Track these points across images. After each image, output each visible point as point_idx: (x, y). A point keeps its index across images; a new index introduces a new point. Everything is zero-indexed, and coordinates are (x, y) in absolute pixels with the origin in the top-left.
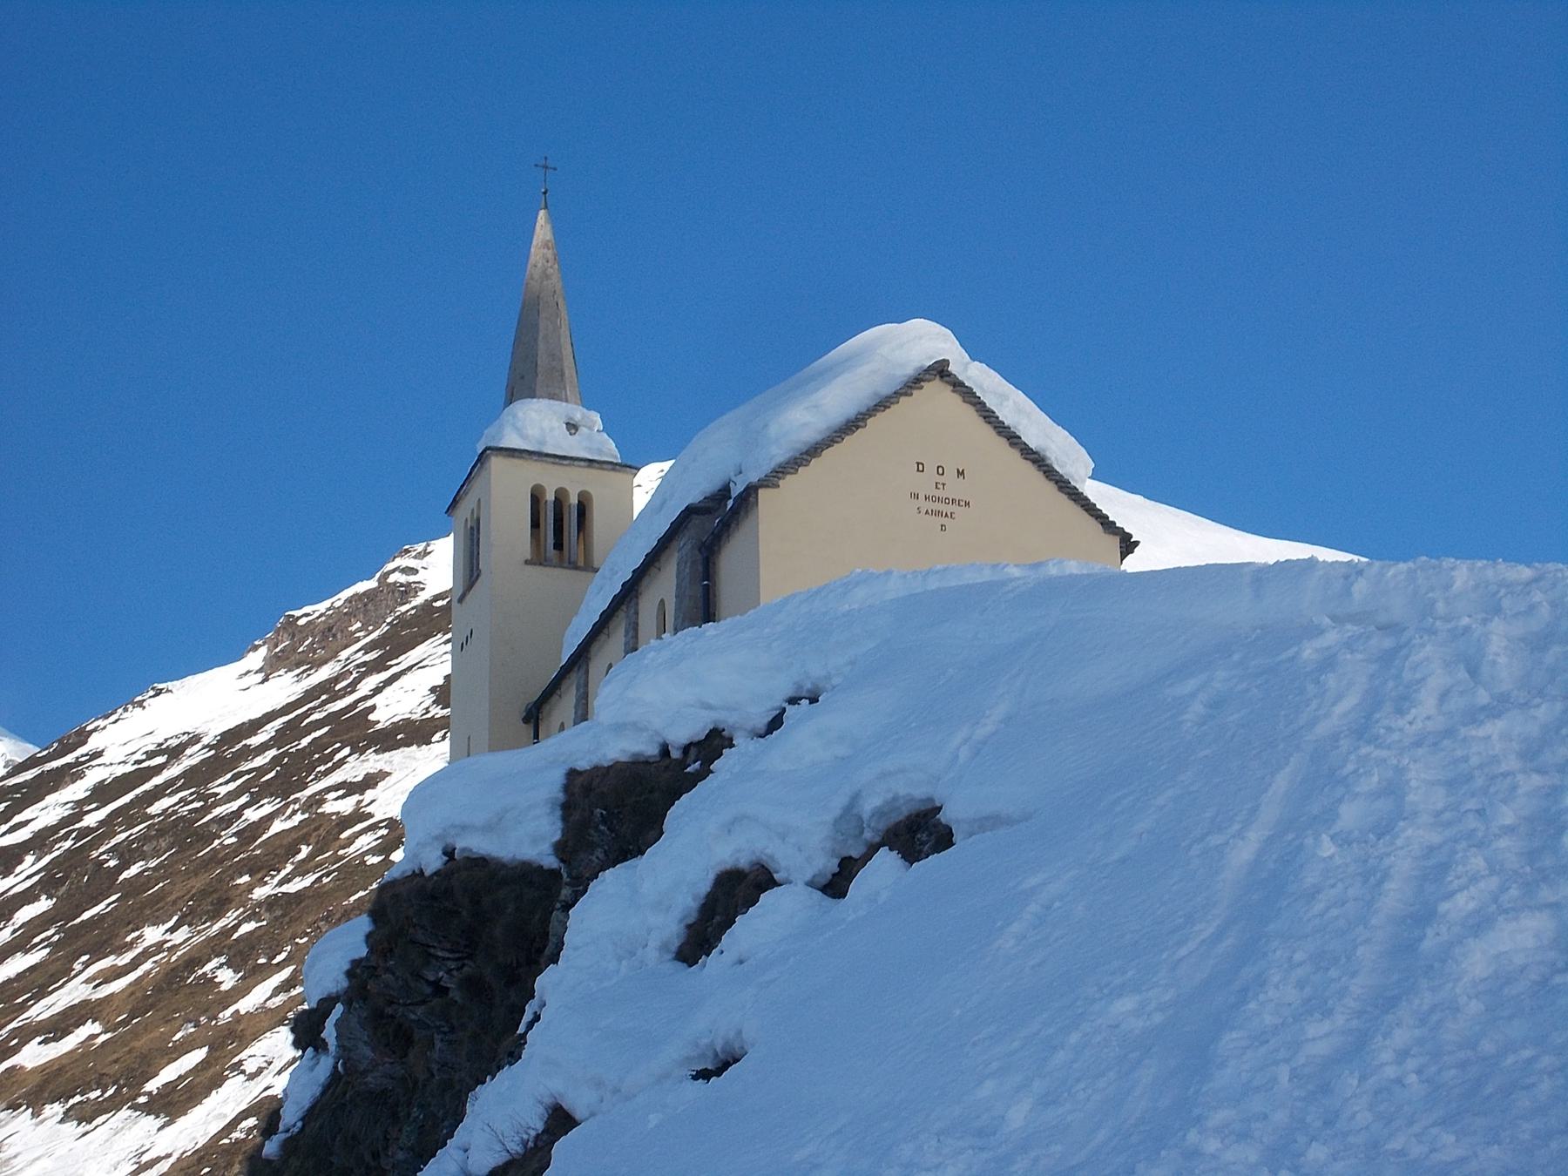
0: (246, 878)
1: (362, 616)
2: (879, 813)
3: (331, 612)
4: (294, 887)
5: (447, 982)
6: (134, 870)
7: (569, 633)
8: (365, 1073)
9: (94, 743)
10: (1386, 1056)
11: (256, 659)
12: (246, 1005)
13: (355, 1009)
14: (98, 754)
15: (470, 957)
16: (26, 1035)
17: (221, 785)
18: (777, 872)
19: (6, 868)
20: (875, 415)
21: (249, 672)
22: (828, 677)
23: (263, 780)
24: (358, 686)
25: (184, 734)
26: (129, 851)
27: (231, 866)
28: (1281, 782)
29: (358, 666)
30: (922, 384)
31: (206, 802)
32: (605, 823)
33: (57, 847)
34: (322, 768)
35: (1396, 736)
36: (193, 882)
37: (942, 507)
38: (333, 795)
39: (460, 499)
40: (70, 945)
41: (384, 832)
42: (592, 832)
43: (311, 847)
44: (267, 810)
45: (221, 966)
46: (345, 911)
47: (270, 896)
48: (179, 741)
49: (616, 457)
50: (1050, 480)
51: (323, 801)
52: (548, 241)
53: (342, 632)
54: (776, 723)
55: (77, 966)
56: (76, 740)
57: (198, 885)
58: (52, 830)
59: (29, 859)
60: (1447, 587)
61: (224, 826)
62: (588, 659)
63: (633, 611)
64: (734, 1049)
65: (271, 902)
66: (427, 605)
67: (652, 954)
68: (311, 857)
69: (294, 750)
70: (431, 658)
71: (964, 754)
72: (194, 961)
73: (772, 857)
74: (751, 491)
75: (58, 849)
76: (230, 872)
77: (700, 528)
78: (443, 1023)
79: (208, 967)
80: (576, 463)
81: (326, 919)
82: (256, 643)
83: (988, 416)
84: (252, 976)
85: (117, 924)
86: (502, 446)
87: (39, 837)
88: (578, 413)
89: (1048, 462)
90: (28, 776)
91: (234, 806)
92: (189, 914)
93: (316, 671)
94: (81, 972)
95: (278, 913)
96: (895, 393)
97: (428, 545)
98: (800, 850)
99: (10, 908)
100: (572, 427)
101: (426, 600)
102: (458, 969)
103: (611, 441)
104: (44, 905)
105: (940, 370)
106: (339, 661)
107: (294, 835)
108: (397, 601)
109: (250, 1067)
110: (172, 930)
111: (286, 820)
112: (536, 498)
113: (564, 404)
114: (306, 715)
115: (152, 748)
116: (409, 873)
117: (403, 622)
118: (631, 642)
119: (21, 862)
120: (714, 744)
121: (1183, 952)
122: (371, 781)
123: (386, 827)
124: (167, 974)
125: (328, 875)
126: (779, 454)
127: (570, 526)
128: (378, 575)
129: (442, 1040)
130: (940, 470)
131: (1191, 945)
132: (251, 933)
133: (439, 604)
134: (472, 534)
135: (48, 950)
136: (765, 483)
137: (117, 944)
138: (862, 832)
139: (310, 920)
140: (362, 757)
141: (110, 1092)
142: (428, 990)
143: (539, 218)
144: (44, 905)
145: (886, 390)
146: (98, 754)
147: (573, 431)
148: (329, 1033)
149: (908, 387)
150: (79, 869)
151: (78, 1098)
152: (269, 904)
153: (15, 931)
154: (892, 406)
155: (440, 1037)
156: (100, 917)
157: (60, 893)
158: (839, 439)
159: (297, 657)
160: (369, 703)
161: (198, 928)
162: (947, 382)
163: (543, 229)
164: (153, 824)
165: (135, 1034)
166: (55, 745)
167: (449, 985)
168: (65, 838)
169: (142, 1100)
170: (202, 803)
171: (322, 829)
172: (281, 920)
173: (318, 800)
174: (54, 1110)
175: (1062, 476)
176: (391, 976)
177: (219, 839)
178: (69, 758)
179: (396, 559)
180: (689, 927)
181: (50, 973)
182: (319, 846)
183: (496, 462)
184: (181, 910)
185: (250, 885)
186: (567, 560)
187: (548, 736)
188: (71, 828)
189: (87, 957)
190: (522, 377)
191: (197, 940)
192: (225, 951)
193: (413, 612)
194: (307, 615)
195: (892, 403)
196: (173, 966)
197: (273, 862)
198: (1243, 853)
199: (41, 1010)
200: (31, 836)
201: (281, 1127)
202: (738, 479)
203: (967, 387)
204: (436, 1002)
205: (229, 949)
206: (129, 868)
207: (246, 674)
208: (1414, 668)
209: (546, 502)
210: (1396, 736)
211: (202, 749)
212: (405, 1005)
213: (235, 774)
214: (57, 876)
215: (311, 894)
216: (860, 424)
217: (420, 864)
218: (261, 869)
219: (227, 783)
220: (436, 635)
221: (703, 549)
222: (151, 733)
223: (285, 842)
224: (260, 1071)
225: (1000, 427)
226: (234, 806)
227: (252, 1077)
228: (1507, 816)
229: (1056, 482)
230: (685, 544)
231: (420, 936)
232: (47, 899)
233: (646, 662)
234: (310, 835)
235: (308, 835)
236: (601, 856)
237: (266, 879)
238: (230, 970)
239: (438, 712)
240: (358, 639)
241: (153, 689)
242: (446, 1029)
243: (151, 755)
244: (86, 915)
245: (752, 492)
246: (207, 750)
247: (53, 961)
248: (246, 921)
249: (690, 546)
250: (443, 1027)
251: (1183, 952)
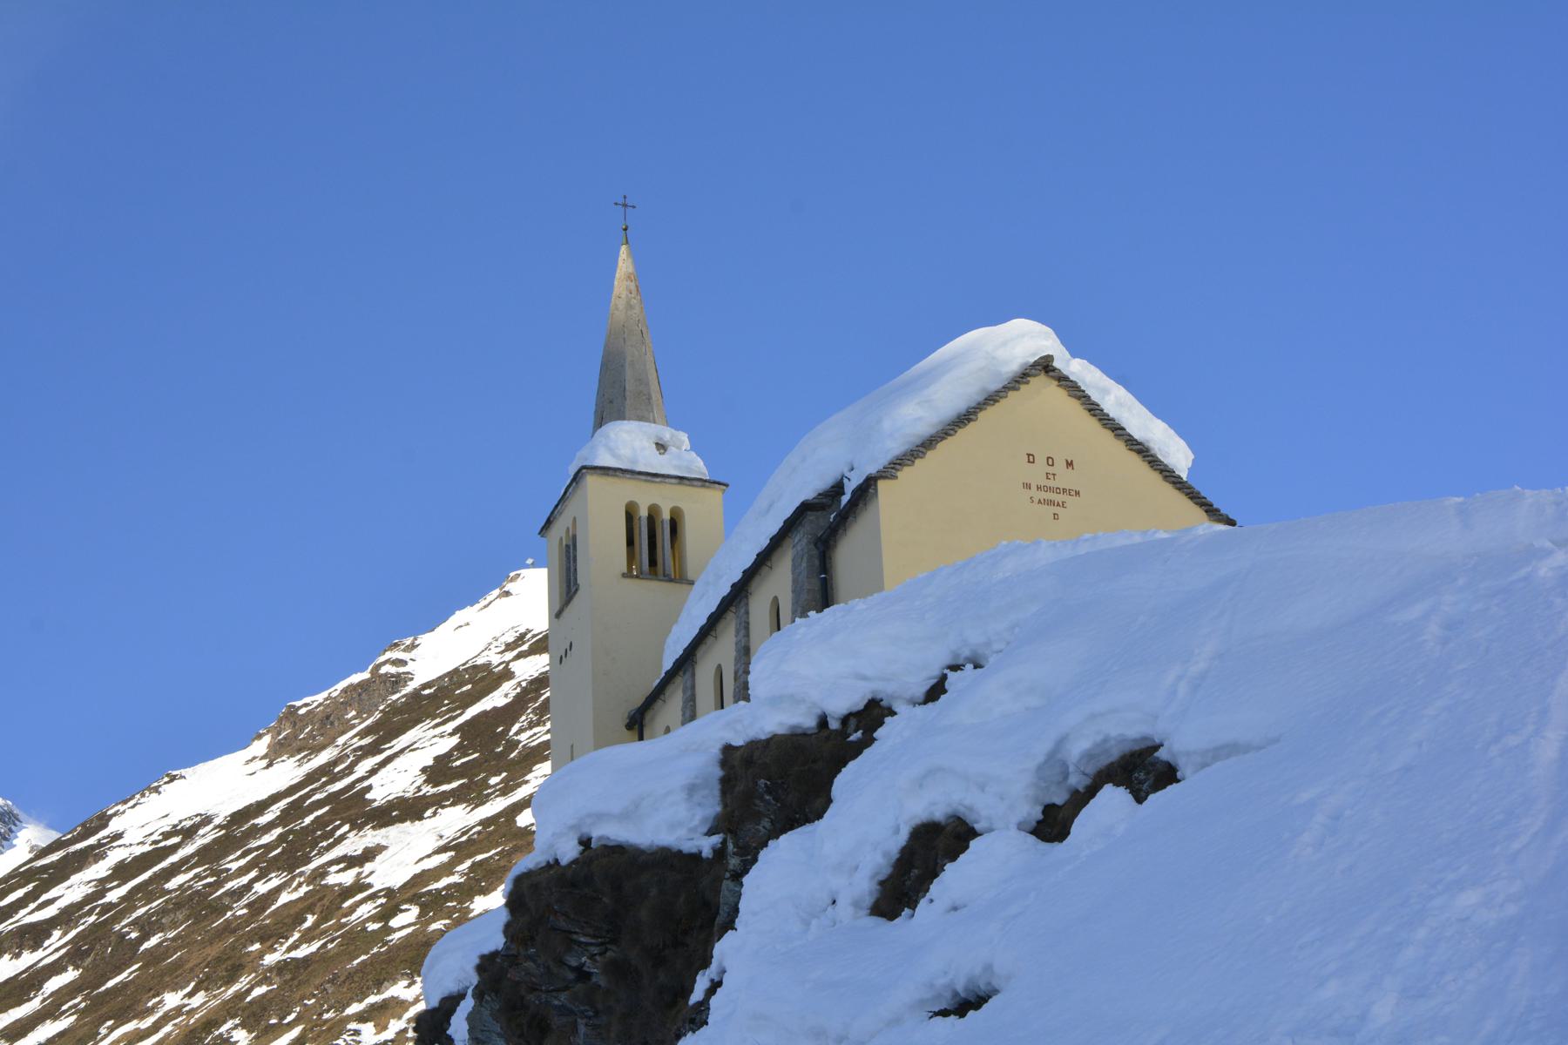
0: (257, 946)
1: (356, 705)
2: (1089, 756)
3: (328, 702)
4: (303, 952)
5: (590, 967)
6: (154, 941)
7: (670, 640)
9: (114, 826)
11: (261, 746)
13: (487, 1002)
14: (118, 836)
15: (614, 941)
17: (232, 861)
18: (977, 822)
19: (36, 943)
20: (986, 409)
21: (254, 758)
22: (988, 644)
23: (270, 856)
24: (356, 769)
25: (196, 816)
26: (149, 923)
27: (243, 935)
29: (355, 750)
30: (1029, 379)
31: (219, 877)
32: (770, 793)
33: (82, 922)
34: (325, 844)
36: (208, 950)
37: (1054, 497)
39: (554, 518)
40: (96, 1011)
41: (383, 900)
42: (757, 802)
43: (316, 916)
44: (275, 883)
45: (236, 1027)
46: (350, 974)
47: (279, 962)
48: (192, 822)
49: (704, 474)
50: (1155, 470)
52: (631, 274)
53: (339, 719)
54: (935, 692)
55: (103, 1031)
56: (98, 823)
57: (214, 953)
59: (57, 934)
61: (236, 898)
63: (743, 611)
64: (979, 987)
65: (281, 967)
66: (416, 694)
67: (844, 911)
68: (316, 925)
69: (297, 828)
70: (422, 741)
72: (211, 1023)
73: (971, 809)
74: (867, 489)
75: (83, 924)
76: (243, 940)
77: (814, 524)
78: (587, 1008)
79: (223, 1029)
80: (667, 480)
81: (331, 981)
82: (261, 732)
83: (1094, 409)
85: (139, 991)
86: (596, 465)
87: (65, 913)
88: (667, 434)
89: (1152, 452)
90: (54, 857)
91: (245, 880)
92: (206, 980)
93: (316, 756)
94: (106, 1036)
95: (288, 977)
96: (1004, 387)
97: (416, 639)
98: (1002, 799)
99: (40, 979)
100: (661, 447)
101: (415, 689)
102: (600, 954)
103: (699, 459)
104: (71, 975)
105: (1045, 366)
106: (337, 746)
107: (300, 906)
108: (387, 690)
110: (191, 995)
111: (292, 892)
112: (630, 517)
113: (653, 425)
114: (308, 796)
115: (168, 829)
116: (544, 864)
117: (394, 709)
118: (743, 641)
119: (49, 936)
120: (873, 714)
121: (1516, 846)
122: (369, 854)
123: (384, 896)
124: (186, 1035)
125: (332, 941)
126: (894, 447)
127: (663, 540)
128: (370, 667)
129: (586, 1025)
130: (1050, 461)
132: (263, 996)
133: (427, 692)
134: (568, 551)
135: (75, 1017)
136: (884, 474)
137: (139, 1009)
139: (317, 982)
140: (361, 833)
142: (571, 976)
143: (621, 252)
144: (71, 975)
145: (995, 386)
146: (118, 836)
147: (662, 451)
149: (1016, 381)
150: (102, 942)
152: (279, 969)
153: (44, 1000)
154: (1001, 400)
155: (584, 1021)
156: (124, 985)
157: (86, 964)
158: (952, 432)
159: (299, 743)
160: (366, 784)
161: (214, 993)
162: (1053, 377)
163: (624, 263)
164: (171, 899)
166: (79, 829)
167: (592, 970)
168: (90, 913)
170: (215, 878)
171: (326, 900)
172: (290, 983)
173: (321, 872)
175: (1166, 465)
176: (532, 964)
177: (231, 910)
178: (92, 841)
179: (387, 653)
181: (77, 1038)
182: (324, 914)
184: (198, 977)
185: (261, 952)
186: (662, 573)
187: (652, 737)
188: (95, 904)
189: (112, 1022)
190: (611, 402)
191: (214, 1003)
192: (240, 1013)
193: (403, 700)
194: (306, 705)
195: (1001, 398)
196: (191, 1028)
197: (281, 931)
200: (57, 912)
202: (851, 475)
203: (1072, 381)
204: (579, 987)
205: (243, 1011)
206: (149, 940)
207: (251, 761)
209: (640, 518)
211: (212, 830)
212: (548, 991)
214: (83, 948)
215: (317, 959)
216: (971, 417)
217: (556, 855)
218: (270, 937)
219: (237, 859)
220: (425, 721)
221: (819, 544)
222: (167, 816)
223: (292, 912)
225: (1105, 419)
229: (1161, 471)
230: (800, 540)
231: (562, 923)
232: (73, 970)
233: (798, 637)
234: (315, 906)
235: (314, 904)
236: (768, 825)
237: (276, 946)
238: (245, 1031)
239: (428, 790)
240: (354, 726)
241: (168, 775)
242: (591, 1013)
243: (166, 836)
244: (110, 984)
245: (872, 482)
246: (218, 830)
247: (80, 1026)
248: (258, 986)
249: (805, 540)
250: (588, 1011)
251: (1516, 846)
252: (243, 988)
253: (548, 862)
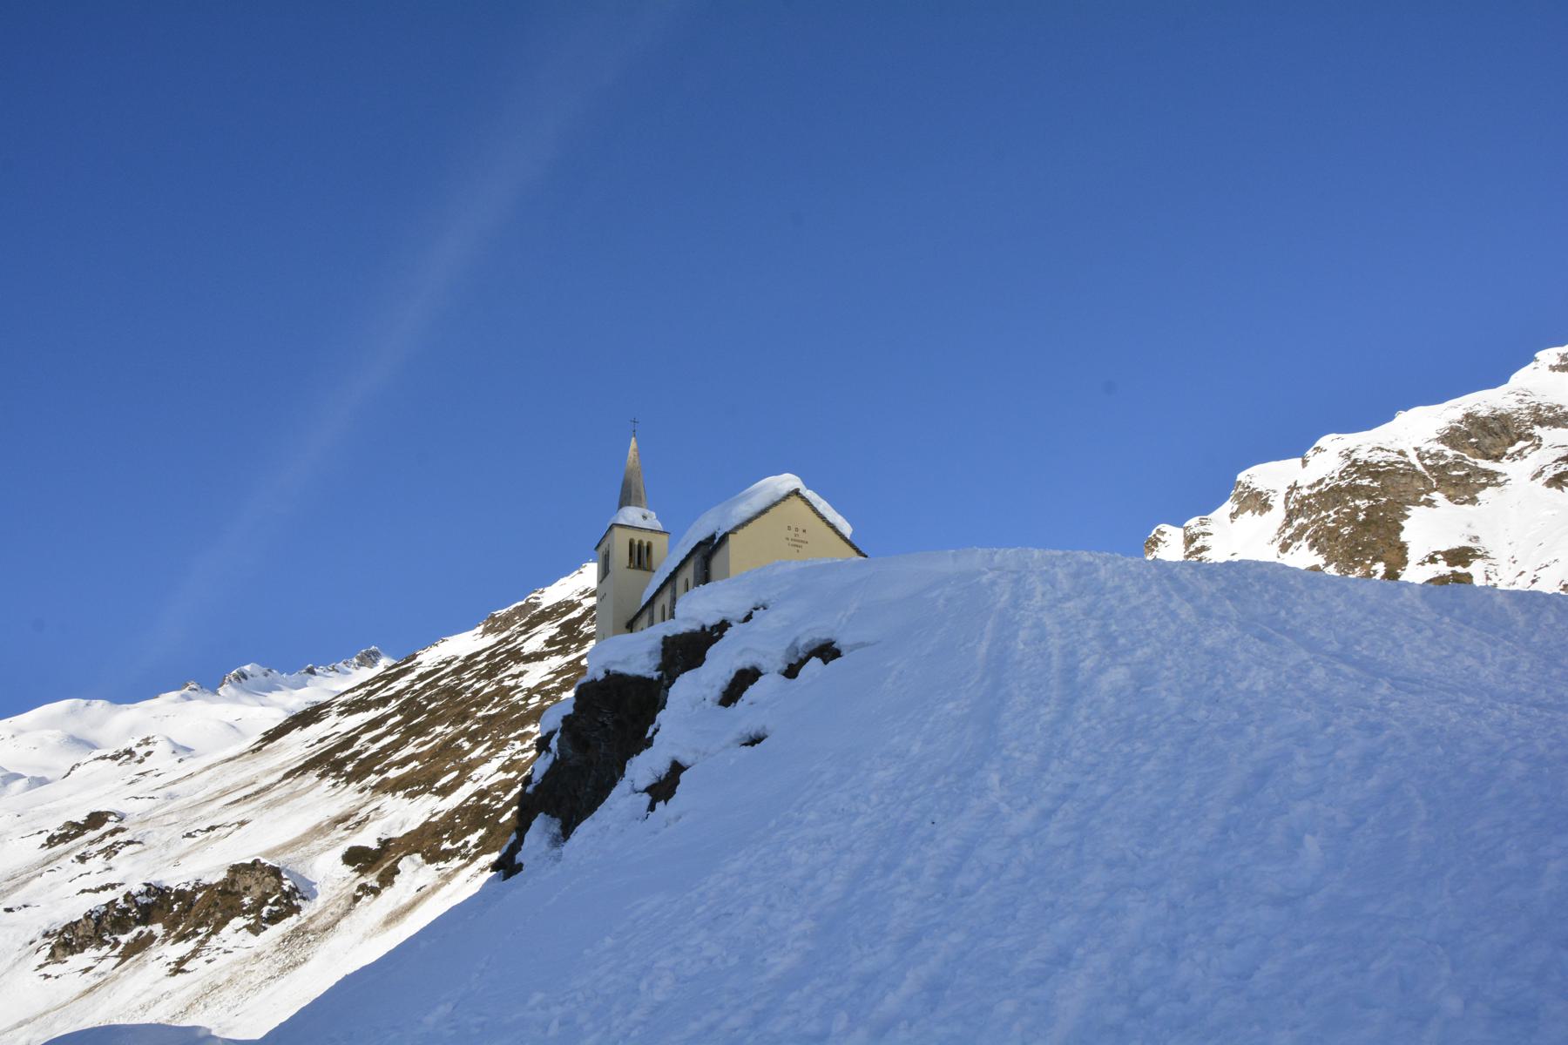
0: (474, 709)
2: (807, 645)
4: (493, 712)
6: (433, 705)
7: (645, 593)
8: (569, 759)
9: (419, 659)
10: (1081, 719)
11: (480, 629)
12: (473, 755)
14: (420, 663)
16: (390, 766)
22: (769, 600)
28: (990, 624)
35: (1032, 607)
37: (798, 544)
38: (507, 679)
51: (503, 681)
54: (748, 618)
55: (411, 740)
58: (402, 691)
59: (393, 701)
60: (1032, 557)
62: (654, 603)
65: (484, 718)
66: (543, 611)
67: (709, 703)
68: (499, 701)
71: (844, 621)
72: (454, 739)
73: (760, 664)
77: (703, 549)
79: (459, 742)
83: (815, 510)
84: (476, 745)
88: (647, 512)
91: (471, 682)
100: (645, 517)
104: (399, 718)
105: (796, 492)
109: (474, 778)
110: (447, 728)
117: (534, 616)
119: (390, 702)
120: (723, 626)
121: (969, 686)
122: (521, 674)
131: (972, 683)
138: (798, 653)
141: (422, 787)
142: (599, 725)
144: (399, 718)
145: (776, 500)
146: (420, 663)
148: (554, 744)
151: (409, 790)
156: (420, 723)
163: (633, 444)
165: (432, 766)
168: (407, 693)
169: (434, 790)
173: (502, 681)
174: (400, 794)
178: (410, 664)
180: (724, 692)
183: (616, 530)
191: (456, 731)
198: (983, 649)
199: (396, 757)
201: (533, 781)
202: (719, 532)
208: (1031, 583)
210: (1032, 607)
213: (347, 749)
218: (480, 705)
224: (478, 779)
226: (471, 682)
227: (475, 782)
228: (1090, 634)
243: (440, 664)
244: (415, 722)
251: (969, 686)
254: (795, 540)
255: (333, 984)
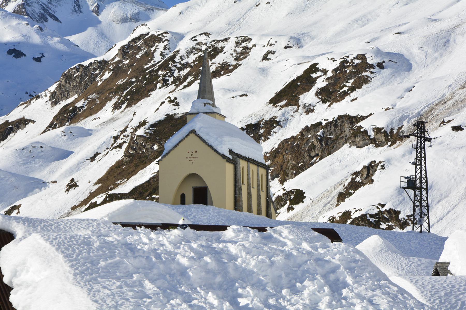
79: (72, 184)
252: (422, 110)
253: (307, 126)
254: (192, 158)
255: (5, 246)
